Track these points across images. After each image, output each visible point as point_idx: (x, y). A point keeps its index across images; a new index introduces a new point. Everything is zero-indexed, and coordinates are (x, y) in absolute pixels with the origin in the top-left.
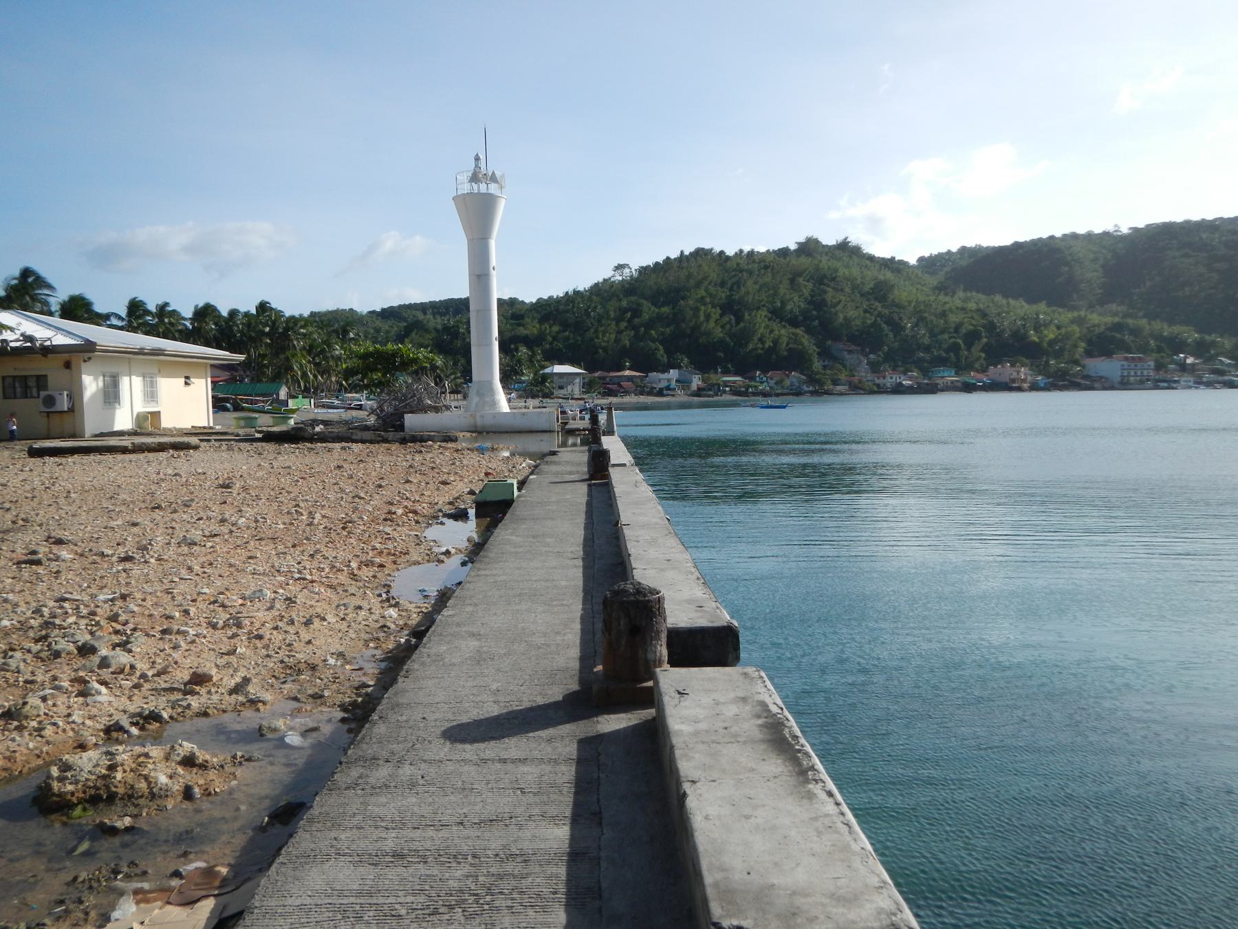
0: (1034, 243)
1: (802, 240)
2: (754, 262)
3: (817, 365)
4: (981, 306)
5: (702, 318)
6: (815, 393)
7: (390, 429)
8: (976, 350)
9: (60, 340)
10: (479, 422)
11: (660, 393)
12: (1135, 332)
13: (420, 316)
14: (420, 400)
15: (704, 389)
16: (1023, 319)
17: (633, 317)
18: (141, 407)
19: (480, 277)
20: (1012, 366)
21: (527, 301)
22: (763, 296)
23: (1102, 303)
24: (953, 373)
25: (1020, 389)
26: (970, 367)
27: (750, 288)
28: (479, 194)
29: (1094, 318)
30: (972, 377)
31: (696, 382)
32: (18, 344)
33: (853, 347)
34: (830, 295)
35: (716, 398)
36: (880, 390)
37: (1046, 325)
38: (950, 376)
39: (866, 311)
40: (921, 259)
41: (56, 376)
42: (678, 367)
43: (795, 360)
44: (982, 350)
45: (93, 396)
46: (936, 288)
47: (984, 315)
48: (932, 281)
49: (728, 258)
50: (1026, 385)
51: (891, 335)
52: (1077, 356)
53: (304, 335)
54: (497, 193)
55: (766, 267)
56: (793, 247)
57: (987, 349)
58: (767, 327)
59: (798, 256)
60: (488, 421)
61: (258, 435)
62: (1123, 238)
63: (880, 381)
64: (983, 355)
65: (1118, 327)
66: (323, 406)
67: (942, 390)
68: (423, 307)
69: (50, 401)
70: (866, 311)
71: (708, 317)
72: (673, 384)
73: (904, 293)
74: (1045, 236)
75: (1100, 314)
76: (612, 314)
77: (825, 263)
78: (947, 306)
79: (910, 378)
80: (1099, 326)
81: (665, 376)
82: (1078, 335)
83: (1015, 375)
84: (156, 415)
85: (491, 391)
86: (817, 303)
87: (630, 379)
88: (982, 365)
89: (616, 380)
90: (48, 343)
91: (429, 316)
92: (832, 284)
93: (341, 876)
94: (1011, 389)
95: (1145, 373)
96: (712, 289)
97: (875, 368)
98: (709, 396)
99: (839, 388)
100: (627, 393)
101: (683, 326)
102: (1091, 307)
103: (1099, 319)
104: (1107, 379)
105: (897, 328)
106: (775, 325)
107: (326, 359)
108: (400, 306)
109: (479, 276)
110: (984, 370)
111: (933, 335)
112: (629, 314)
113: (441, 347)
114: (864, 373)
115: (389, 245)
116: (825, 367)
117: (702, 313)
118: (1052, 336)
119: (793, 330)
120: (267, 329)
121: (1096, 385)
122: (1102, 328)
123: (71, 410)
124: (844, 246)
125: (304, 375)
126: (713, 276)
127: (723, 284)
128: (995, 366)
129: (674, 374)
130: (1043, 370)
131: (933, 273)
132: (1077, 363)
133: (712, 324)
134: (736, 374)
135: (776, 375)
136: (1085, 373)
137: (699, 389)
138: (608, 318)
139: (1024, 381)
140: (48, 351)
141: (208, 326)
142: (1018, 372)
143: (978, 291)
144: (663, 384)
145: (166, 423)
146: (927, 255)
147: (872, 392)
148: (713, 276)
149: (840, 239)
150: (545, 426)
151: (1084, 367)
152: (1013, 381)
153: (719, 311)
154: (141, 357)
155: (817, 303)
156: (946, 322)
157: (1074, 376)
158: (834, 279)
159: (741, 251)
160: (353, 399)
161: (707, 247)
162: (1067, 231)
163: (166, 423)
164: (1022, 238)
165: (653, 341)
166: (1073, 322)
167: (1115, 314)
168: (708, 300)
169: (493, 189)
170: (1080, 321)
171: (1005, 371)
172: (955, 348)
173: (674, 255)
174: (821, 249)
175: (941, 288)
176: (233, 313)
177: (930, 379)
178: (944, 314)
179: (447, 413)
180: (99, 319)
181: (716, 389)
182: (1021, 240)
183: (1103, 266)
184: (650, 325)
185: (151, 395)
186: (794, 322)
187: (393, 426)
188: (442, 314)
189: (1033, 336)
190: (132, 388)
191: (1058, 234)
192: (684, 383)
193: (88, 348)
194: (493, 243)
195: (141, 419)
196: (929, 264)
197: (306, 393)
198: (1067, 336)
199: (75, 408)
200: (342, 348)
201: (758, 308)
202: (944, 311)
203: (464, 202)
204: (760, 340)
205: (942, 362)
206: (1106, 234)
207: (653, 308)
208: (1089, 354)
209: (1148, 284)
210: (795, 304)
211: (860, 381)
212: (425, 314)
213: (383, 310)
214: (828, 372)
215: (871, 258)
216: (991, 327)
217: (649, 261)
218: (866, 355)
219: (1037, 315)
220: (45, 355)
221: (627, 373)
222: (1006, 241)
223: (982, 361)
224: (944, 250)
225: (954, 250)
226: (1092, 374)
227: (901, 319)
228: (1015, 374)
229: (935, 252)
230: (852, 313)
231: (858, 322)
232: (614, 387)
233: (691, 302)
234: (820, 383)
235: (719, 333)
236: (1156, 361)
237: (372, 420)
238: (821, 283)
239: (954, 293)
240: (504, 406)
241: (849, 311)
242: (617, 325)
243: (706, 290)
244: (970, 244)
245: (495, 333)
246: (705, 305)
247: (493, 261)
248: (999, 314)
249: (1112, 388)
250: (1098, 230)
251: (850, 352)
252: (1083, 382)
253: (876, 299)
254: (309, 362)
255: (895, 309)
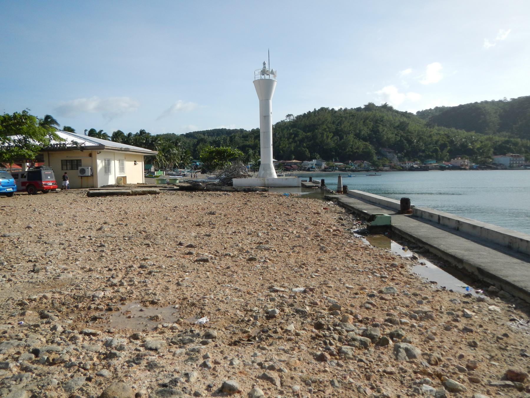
0: (468, 105)
1: (367, 104)
2: (347, 113)
3: (375, 158)
4: (446, 133)
5: (325, 137)
6: (375, 170)
7: (226, 185)
8: (445, 152)
9: (88, 144)
10: (266, 182)
11: (308, 170)
12: (516, 144)
13: (202, 136)
14: (238, 172)
15: (327, 168)
16: (465, 138)
17: (295, 137)
18: (118, 175)
19: (265, 117)
20: (461, 159)
21: (248, 130)
22: (352, 128)
23: (499, 131)
24: (435, 162)
25: (465, 169)
26: (442, 159)
27: (346, 125)
28: (265, 80)
29: (497, 138)
30: (444, 163)
31: (324, 165)
32: (70, 146)
33: (391, 150)
34: (381, 128)
35: (332, 172)
36: (403, 169)
37: (476, 141)
38: (434, 164)
39: (396, 135)
40: (418, 112)
41: (85, 161)
42: (315, 158)
43: (366, 156)
44: (448, 152)
45: (101, 169)
46: (425, 125)
47: (448, 137)
48: (424, 122)
49: (336, 112)
50: (467, 167)
51: (407, 145)
52: (490, 155)
53: (160, 144)
54: (273, 79)
55: (353, 116)
56: (363, 107)
57: (450, 152)
58: (353, 141)
59: (365, 111)
60: (271, 182)
61: (175, 187)
62: (508, 103)
63: (404, 165)
64: (448, 154)
65: (507, 142)
66: (169, 175)
67: (431, 169)
68: (203, 133)
69: (83, 171)
70: (396, 135)
71: (328, 137)
72: (314, 166)
73: (413, 127)
74: (473, 102)
75: (499, 137)
76: (286, 136)
77: (378, 114)
78: (432, 133)
79: (417, 164)
80: (499, 141)
81: (311, 162)
82: (489, 146)
83: (463, 163)
84: (125, 178)
85: (270, 168)
86: (375, 131)
87: (295, 163)
88: (447, 158)
89: (290, 164)
90: (83, 145)
91: (206, 137)
92: (381, 123)
93: (161, 362)
94: (461, 169)
95: (521, 162)
96: (329, 125)
97: (400, 159)
98: (329, 171)
99: (385, 168)
100: (294, 170)
101: (317, 141)
102: (494, 133)
103: (499, 138)
104: (503, 165)
105: (410, 142)
106: (356, 141)
107: (170, 155)
108: (194, 132)
109: (265, 117)
110: (448, 161)
111: (426, 145)
112: (293, 136)
113: (243, 148)
114: (396, 161)
115: (179, 106)
116: (379, 159)
117: (325, 135)
118: (479, 146)
119: (365, 143)
120: (144, 141)
121: (499, 168)
122: (500, 143)
123: (92, 175)
124: (385, 106)
125: (161, 160)
126: (329, 119)
127: (333, 123)
128: (454, 159)
129: (314, 161)
130: (475, 161)
131: (423, 118)
132: (490, 157)
133: (329, 140)
134: (341, 162)
135: (358, 162)
136: (494, 162)
137: (325, 168)
138: (284, 137)
139: (467, 165)
140: (83, 149)
141: (142, 139)
142: (464, 162)
143: (444, 126)
144: (310, 166)
145: (129, 182)
146: (421, 110)
147: (400, 170)
148: (329, 119)
149: (384, 103)
150: (296, 185)
151: (493, 159)
152: (462, 165)
153: (332, 134)
154: (120, 152)
155: (375, 131)
156: (432, 140)
157: (489, 163)
158: (382, 121)
159: (341, 109)
160: (181, 172)
161: (326, 107)
162: (483, 100)
163: (129, 182)
164: (463, 103)
165: (304, 147)
166: (487, 140)
167: (505, 137)
168: (327, 130)
169: (271, 77)
170: (490, 139)
171: (458, 161)
172: (436, 151)
173: (312, 110)
174: (375, 108)
175: (428, 125)
176: (130, 134)
177: (425, 164)
178: (430, 136)
179: (244, 179)
180: (105, 136)
181: (333, 168)
182: (463, 104)
183: (499, 115)
184: (302, 141)
185: (122, 169)
186: (365, 139)
187: (227, 184)
188: (212, 136)
189: (470, 146)
190: (115, 165)
191: (479, 101)
192: (318, 165)
193: (101, 147)
194: (271, 102)
195: (119, 179)
196: (422, 114)
197: (162, 168)
198: (485, 146)
199: (93, 175)
200: (177, 150)
201: (349, 134)
202: (431, 135)
203: (257, 83)
204: (352, 148)
205: (429, 157)
206: (500, 101)
207: (304, 133)
208: (495, 154)
209: (520, 123)
210: (365, 131)
211: (395, 165)
212: (204, 135)
213: (187, 134)
214: (381, 161)
215: (397, 112)
216: (452, 142)
217: (301, 113)
218: (397, 154)
219: (472, 137)
220: (82, 151)
221: (294, 161)
222: (456, 104)
223: (447, 156)
224: (428, 108)
225: (433, 108)
226: (497, 162)
227: (412, 138)
228: (463, 162)
229: (424, 109)
230: (390, 136)
231: (393, 140)
232: (289, 167)
233: (320, 131)
234: (378, 166)
235: (332, 145)
236: (525, 157)
237: (217, 181)
238: (376, 123)
239: (434, 127)
240: (275, 175)
241: (389, 135)
242: (288, 140)
243: (326, 125)
244: (440, 105)
245: (271, 143)
246: (326, 132)
247: (271, 110)
248: (455, 136)
249: (506, 169)
250: (497, 99)
251: (389, 152)
252: (492, 166)
253: (400, 129)
254: (163, 155)
255: (409, 134)
